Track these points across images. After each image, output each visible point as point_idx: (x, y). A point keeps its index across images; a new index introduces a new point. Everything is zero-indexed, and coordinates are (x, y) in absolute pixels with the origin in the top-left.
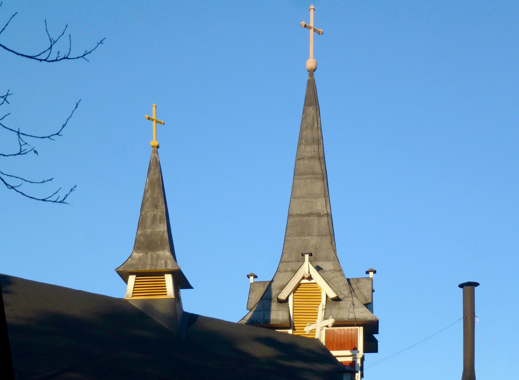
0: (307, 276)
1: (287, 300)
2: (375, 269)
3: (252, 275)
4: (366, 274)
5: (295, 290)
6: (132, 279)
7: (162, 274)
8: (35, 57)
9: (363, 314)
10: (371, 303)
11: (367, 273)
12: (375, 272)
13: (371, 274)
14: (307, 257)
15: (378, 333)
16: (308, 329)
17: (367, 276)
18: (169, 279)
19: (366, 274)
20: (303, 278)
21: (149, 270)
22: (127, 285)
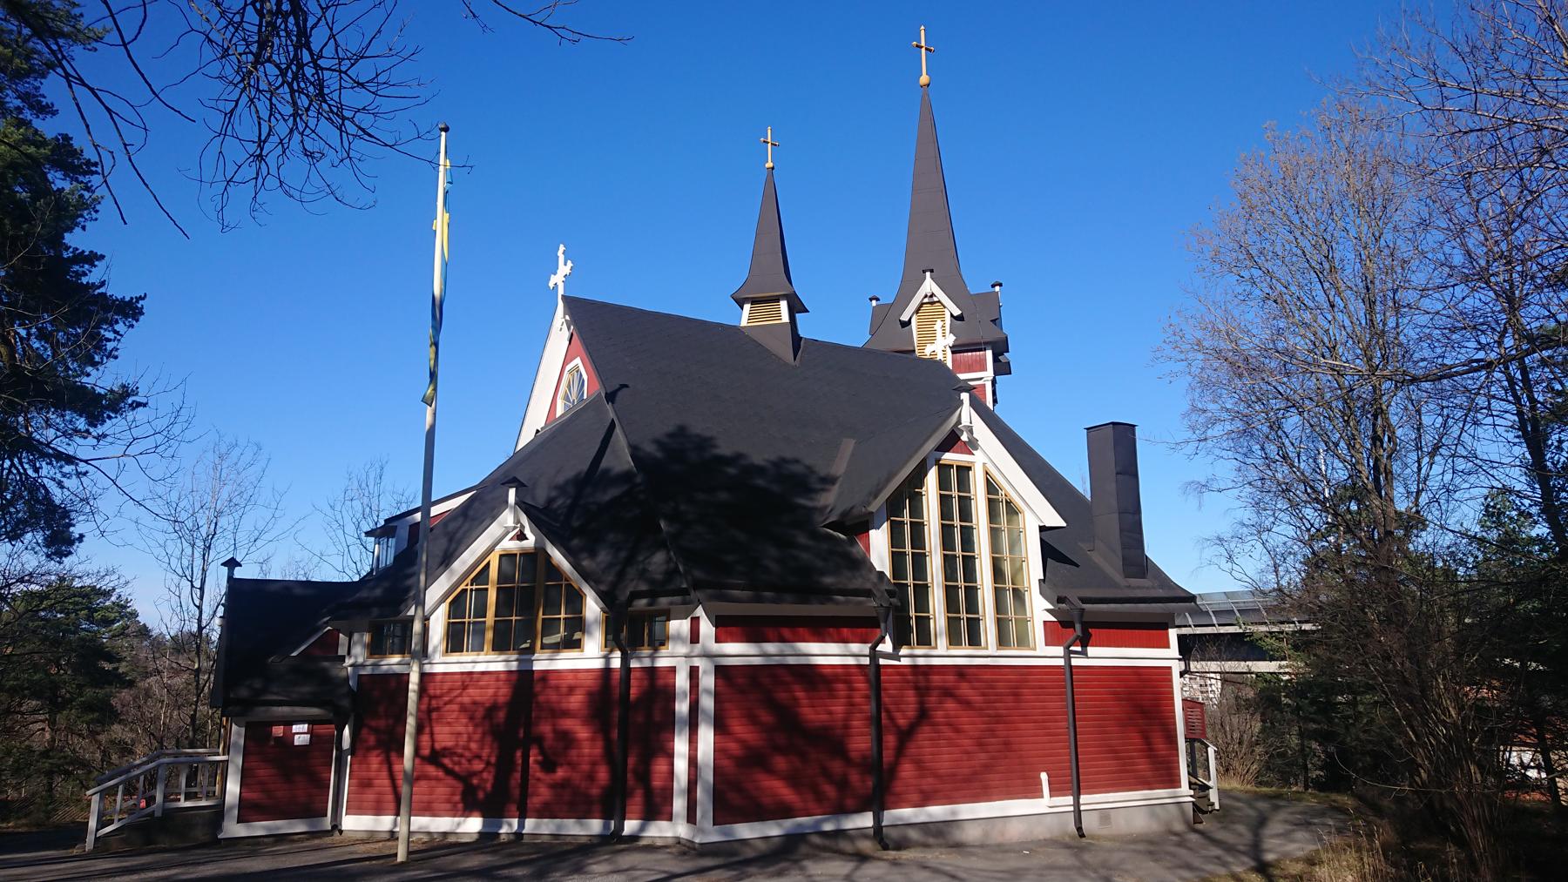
0: (929, 295)
1: (909, 322)
2: (1001, 282)
3: (874, 299)
4: (1046, 645)
5: (917, 311)
6: (747, 307)
7: (777, 299)
8: (114, 115)
9: (990, 334)
10: (999, 318)
11: (993, 286)
12: (1000, 285)
13: (997, 288)
14: (928, 274)
15: (1045, 622)
16: (928, 350)
17: (992, 290)
18: (784, 305)
19: (1046, 645)
20: (926, 296)
21: (565, 569)
22: (742, 309)
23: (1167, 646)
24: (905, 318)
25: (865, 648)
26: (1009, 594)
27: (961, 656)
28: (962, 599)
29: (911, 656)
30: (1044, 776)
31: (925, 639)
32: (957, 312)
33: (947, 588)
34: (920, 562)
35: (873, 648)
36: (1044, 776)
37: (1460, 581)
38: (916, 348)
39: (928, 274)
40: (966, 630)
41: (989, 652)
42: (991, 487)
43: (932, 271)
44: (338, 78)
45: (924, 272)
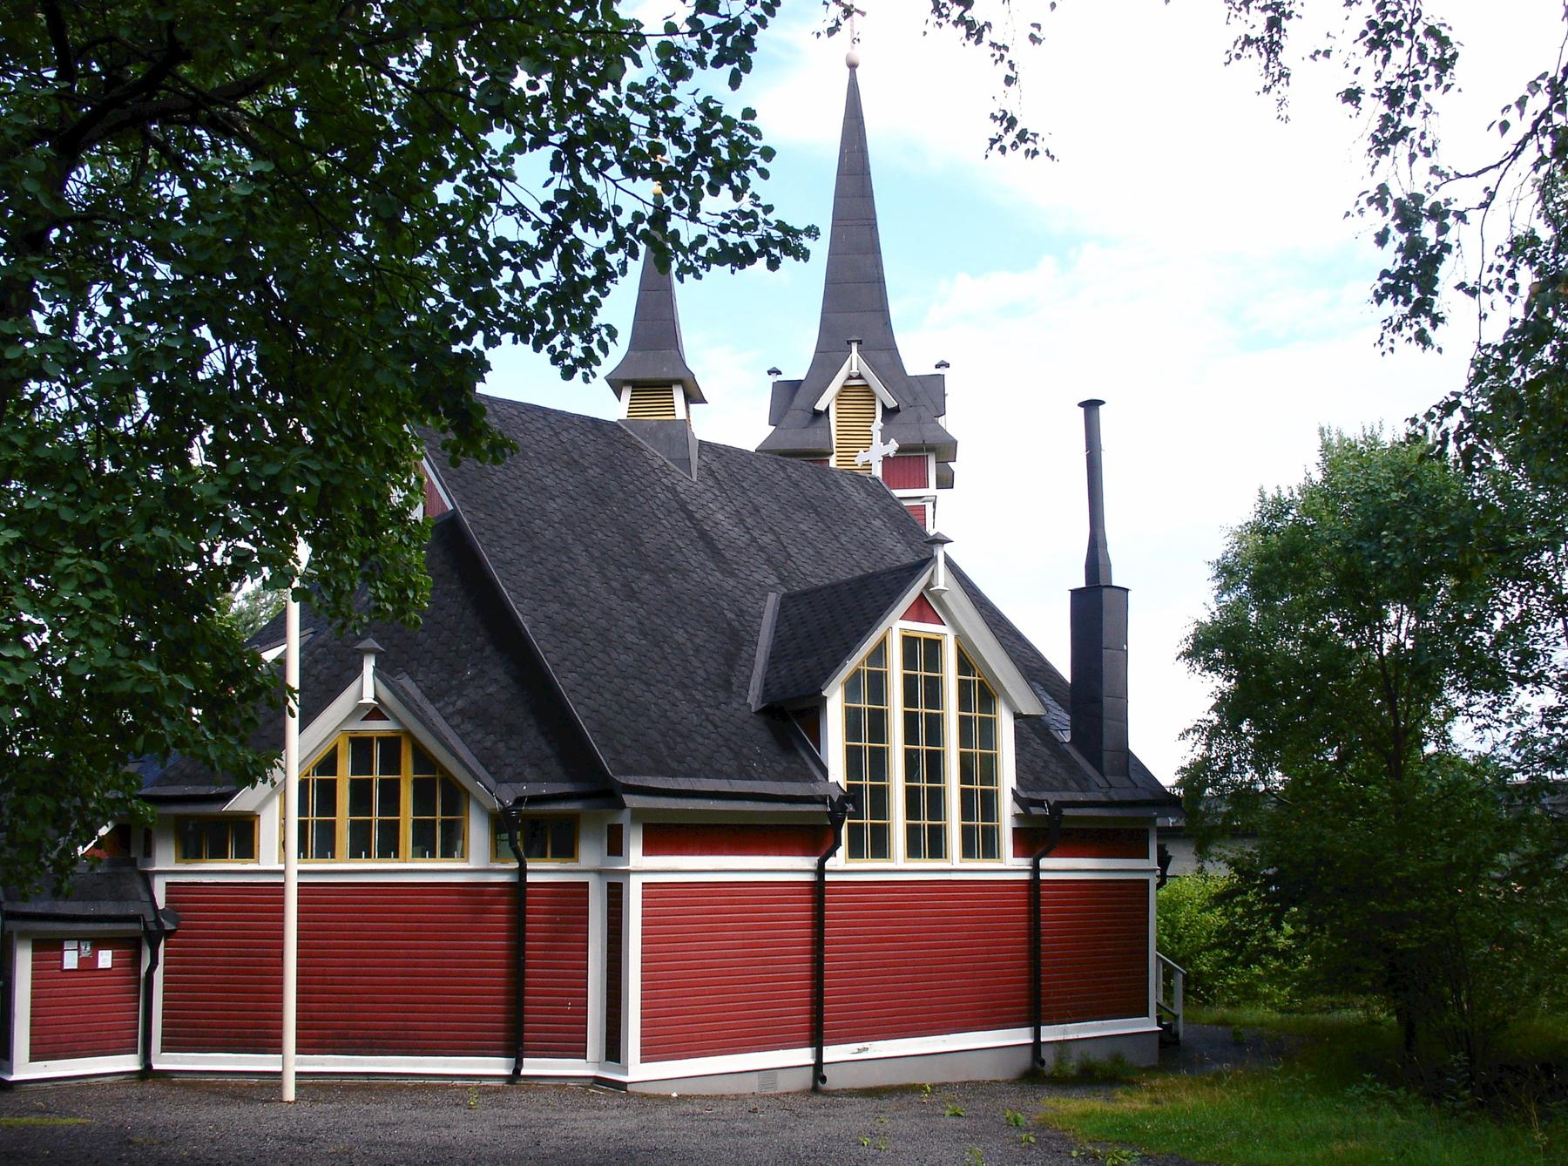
14: (854, 347)
23: (1147, 857)
24: (820, 406)
25: (809, 862)
26: (980, 804)
27: (925, 868)
28: (926, 802)
29: (868, 869)
30: (286, 508)
31: (881, 848)
32: (891, 403)
33: (849, 750)
34: (879, 761)
35: (821, 864)
36: (286, 508)
37: (1477, 817)
38: (835, 450)
39: (854, 347)
40: (927, 842)
41: (955, 864)
42: (964, 665)
43: (860, 342)
44: (611, 185)
45: (849, 343)
